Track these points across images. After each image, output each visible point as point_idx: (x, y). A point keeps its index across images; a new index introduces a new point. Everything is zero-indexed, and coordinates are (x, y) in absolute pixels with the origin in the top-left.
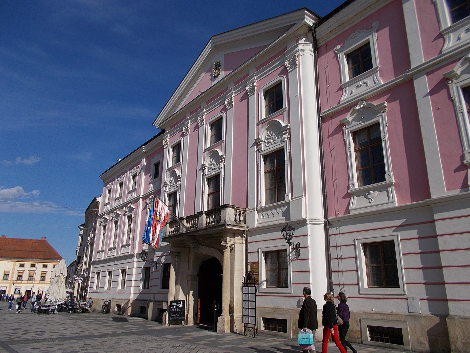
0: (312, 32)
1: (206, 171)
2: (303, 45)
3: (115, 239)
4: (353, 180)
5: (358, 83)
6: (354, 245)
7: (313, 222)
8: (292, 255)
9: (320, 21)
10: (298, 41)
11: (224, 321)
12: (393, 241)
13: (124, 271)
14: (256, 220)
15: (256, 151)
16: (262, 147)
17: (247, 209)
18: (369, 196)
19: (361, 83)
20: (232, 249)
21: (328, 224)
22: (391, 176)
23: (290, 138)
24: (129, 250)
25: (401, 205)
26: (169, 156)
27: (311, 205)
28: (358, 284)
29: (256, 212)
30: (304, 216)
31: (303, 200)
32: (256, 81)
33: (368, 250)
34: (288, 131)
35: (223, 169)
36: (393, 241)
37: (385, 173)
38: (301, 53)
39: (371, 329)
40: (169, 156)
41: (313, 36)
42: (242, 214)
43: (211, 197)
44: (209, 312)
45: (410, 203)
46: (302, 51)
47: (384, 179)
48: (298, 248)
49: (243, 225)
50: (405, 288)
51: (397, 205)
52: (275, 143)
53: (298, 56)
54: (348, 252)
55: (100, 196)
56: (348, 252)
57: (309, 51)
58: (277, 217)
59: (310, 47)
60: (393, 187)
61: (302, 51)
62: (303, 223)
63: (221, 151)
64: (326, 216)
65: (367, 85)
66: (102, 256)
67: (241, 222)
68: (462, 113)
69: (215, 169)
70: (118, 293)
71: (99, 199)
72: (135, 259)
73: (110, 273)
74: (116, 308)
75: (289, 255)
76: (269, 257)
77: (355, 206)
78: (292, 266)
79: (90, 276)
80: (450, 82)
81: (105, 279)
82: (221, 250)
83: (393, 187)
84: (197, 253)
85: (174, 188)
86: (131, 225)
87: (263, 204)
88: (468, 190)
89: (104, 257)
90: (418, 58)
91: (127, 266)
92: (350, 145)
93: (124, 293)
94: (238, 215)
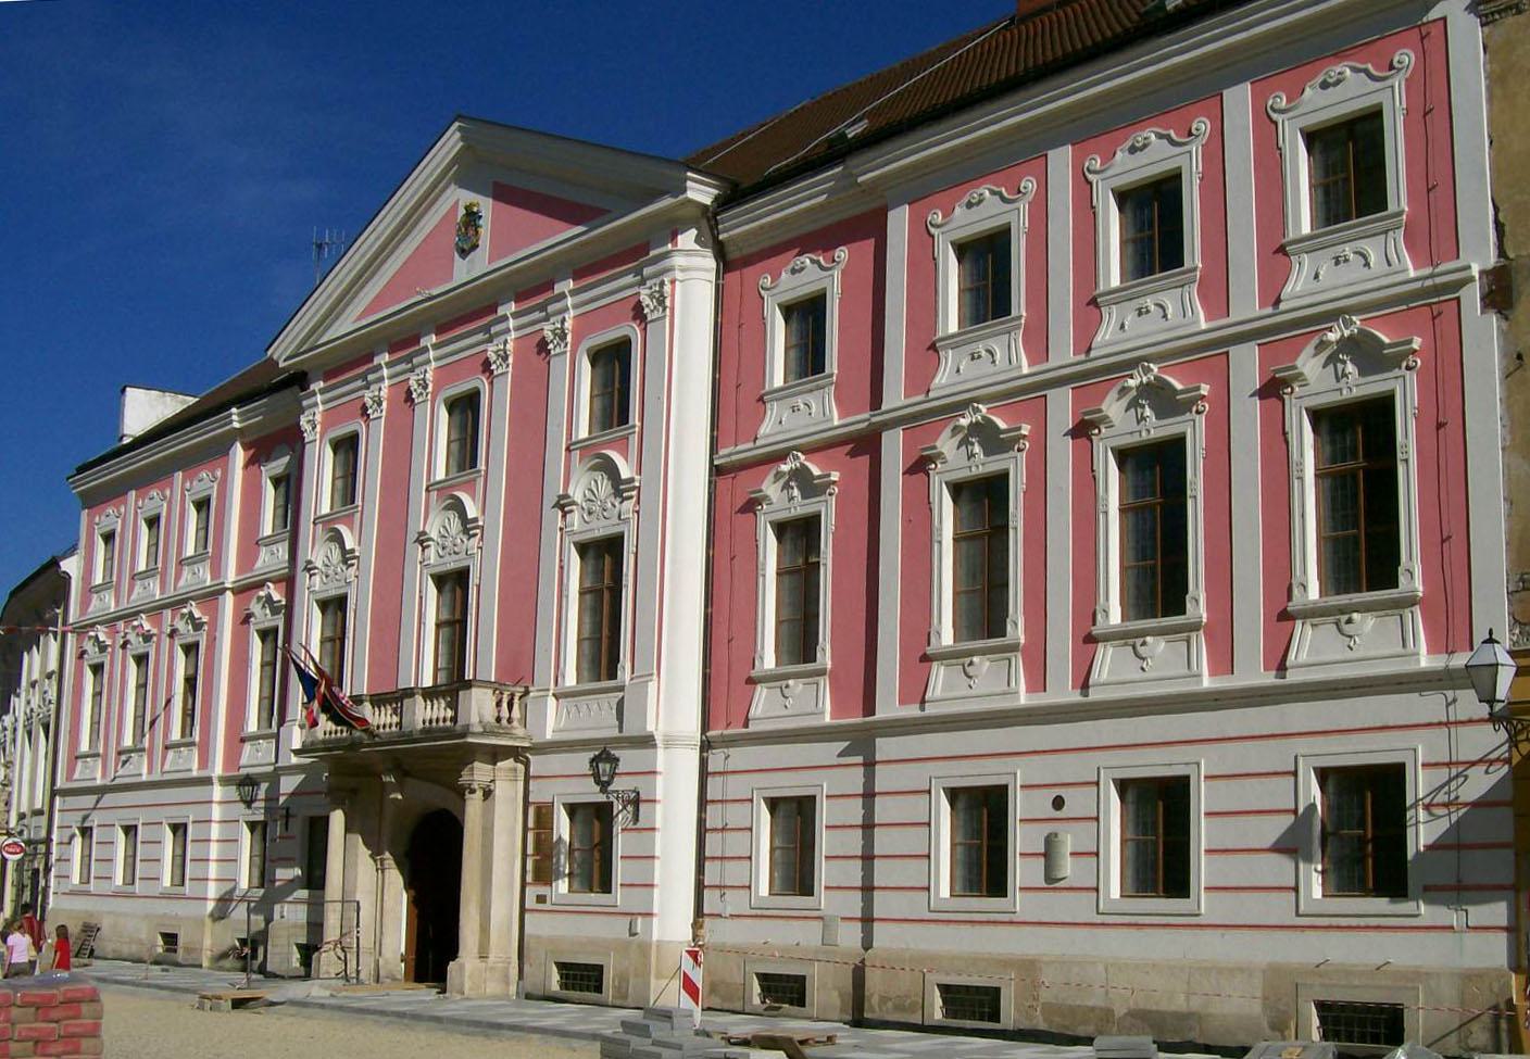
0: (708, 220)
1: (432, 552)
2: (688, 253)
3: (95, 723)
4: (1107, 599)
5: (1141, 300)
6: (1295, 774)
7: (670, 743)
8: (621, 819)
9: (725, 202)
10: (673, 237)
11: (466, 967)
12: (1005, 787)
13: (179, 829)
14: (552, 720)
15: (561, 529)
16: (575, 519)
17: (531, 689)
18: (1347, 628)
19: (1348, 249)
20: (488, 794)
21: (706, 746)
22: (825, 657)
23: (638, 512)
24: (191, 764)
25: (1213, 686)
26: (322, 468)
27: (671, 700)
28: (1296, 889)
29: (551, 701)
30: (650, 728)
31: (652, 686)
32: (570, 315)
33: (1130, 797)
34: (634, 493)
35: (354, 585)
36: (1005, 787)
37: (1398, 563)
38: (678, 275)
39: (764, 978)
40: (322, 468)
41: (713, 234)
42: (516, 700)
43: (445, 631)
44: (434, 949)
45: (860, 720)
46: (683, 270)
47: (1393, 583)
48: (636, 802)
49: (520, 731)
50: (823, 899)
51: (828, 719)
52: (455, 553)
53: (673, 282)
54: (913, 808)
55: (72, 555)
56: (913, 808)
57: (706, 270)
58: (597, 719)
59: (709, 262)
60: (1417, 610)
61: (683, 270)
62: (647, 742)
63: (474, 499)
64: (705, 726)
65: (1367, 264)
66: (93, 770)
67: (515, 724)
68: (1301, 479)
69: (455, 553)
70: (116, 895)
71: (71, 566)
72: (218, 792)
73: (130, 830)
74: (757, 989)
75: (617, 815)
76: (579, 817)
77: (1304, 657)
78: (621, 843)
79: (55, 837)
80: (1096, 431)
81: (239, 851)
82: (461, 792)
83: (1202, 632)
84: (400, 796)
85: (337, 584)
86: (100, 694)
87: (570, 680)
88: (1284, 678)
89: (104, 775)
90: (896, 396)
91: (189, 815)
92: (1302, 455)
93: (87, 894)
94: (505, 705)
